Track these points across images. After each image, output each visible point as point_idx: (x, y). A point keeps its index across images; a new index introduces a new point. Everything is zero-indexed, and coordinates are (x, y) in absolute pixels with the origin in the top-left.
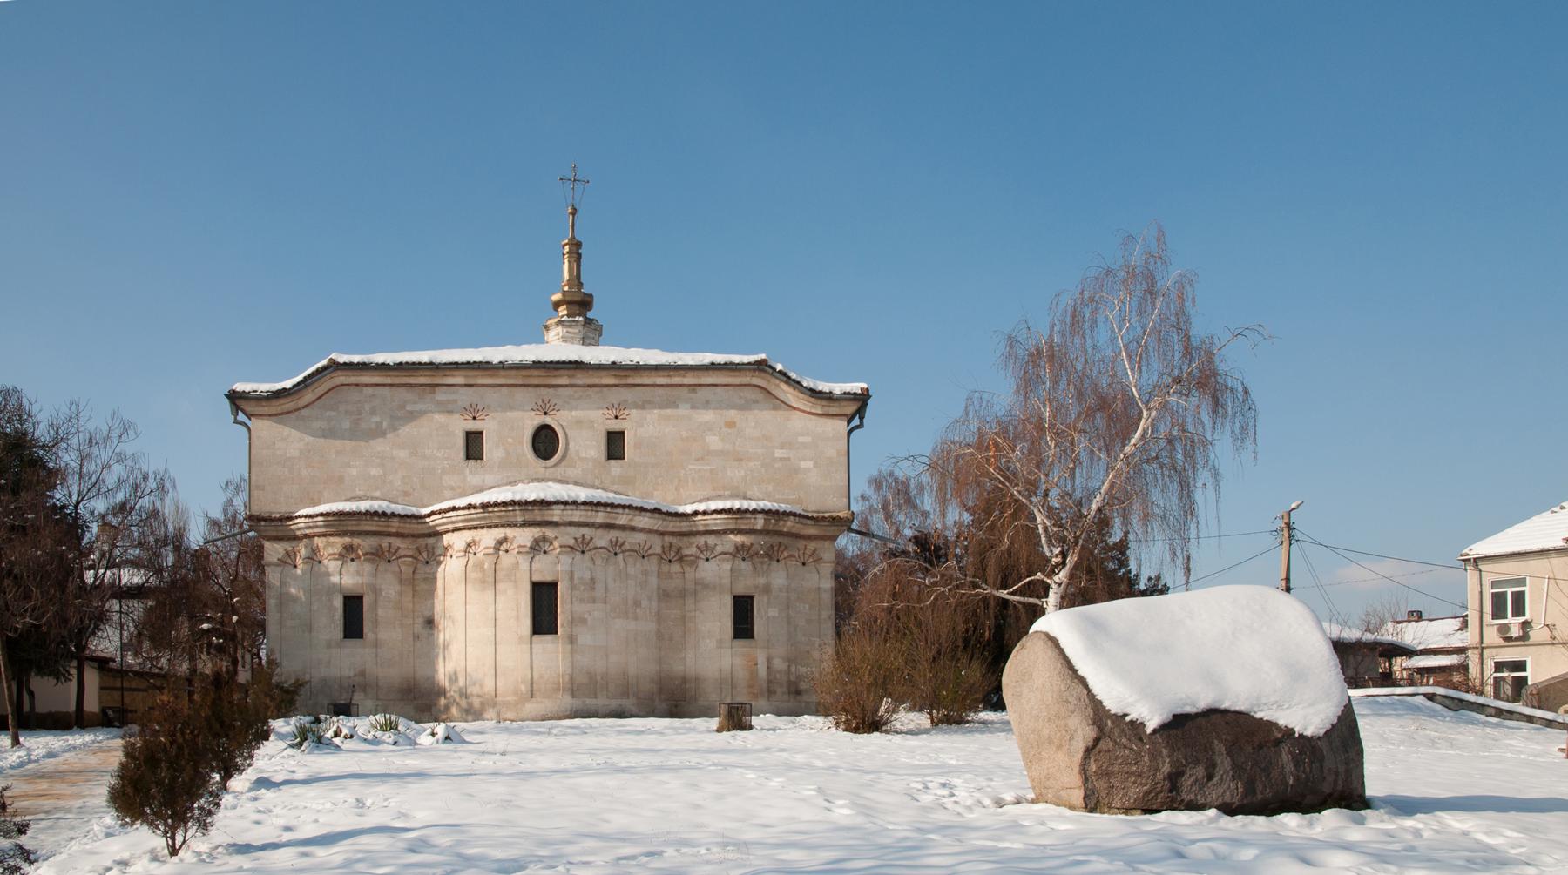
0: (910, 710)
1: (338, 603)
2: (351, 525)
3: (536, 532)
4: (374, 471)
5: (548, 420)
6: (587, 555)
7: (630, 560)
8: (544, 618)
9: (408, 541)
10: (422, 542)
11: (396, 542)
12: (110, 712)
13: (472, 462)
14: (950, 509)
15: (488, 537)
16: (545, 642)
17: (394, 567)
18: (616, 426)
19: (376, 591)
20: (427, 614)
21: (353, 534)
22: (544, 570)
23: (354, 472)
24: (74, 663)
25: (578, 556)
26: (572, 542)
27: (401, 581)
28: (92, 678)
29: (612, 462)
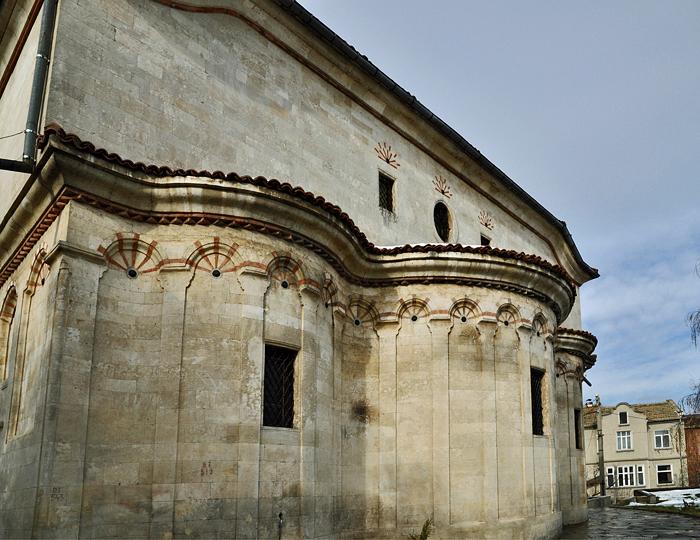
1: (258, 357)
15: (490, 301)
20: (356, 398)
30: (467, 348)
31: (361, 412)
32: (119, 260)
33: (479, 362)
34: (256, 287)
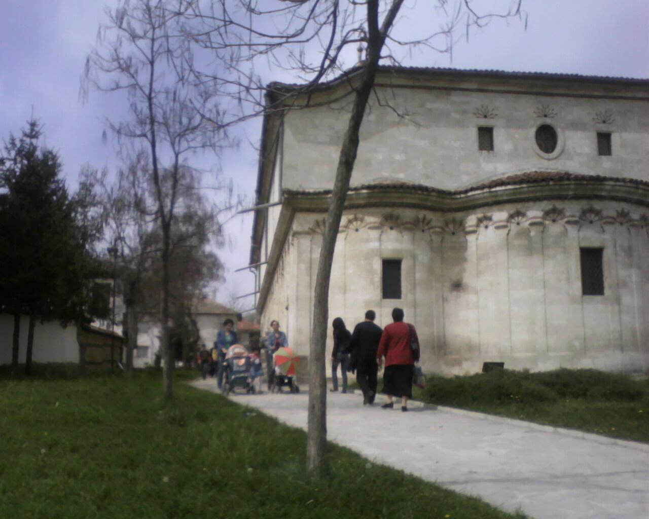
0: (42, 323)
1: (378, 266)
2: (394, 197)
3: (584, 204)
4: (398, 157)
5: (548, 121)
6: (625, 226)
7: (633, 230)
8: (592, 278)
9: (439, 214)
10: (450, 216)
11: (429, 215)
12: (61, 192)
13: (485, 153)
14: (41, 356)
16: (595, 301)
17: (426, 236)
18: (604, 128)
19: (414, 257)
20: (454, 278)
21: (393, 205)
22: (591, 237)
23: (380, 157)
24: (248, 414)
25: (618, 226)
26: (614, 214)
27: (432, 249)
28: (149, 249)
29: (603, 157)
30: (522, 242)
31: (457, 286)
32: (318, 230)
33: (530, 250)
34: (375, 234)
